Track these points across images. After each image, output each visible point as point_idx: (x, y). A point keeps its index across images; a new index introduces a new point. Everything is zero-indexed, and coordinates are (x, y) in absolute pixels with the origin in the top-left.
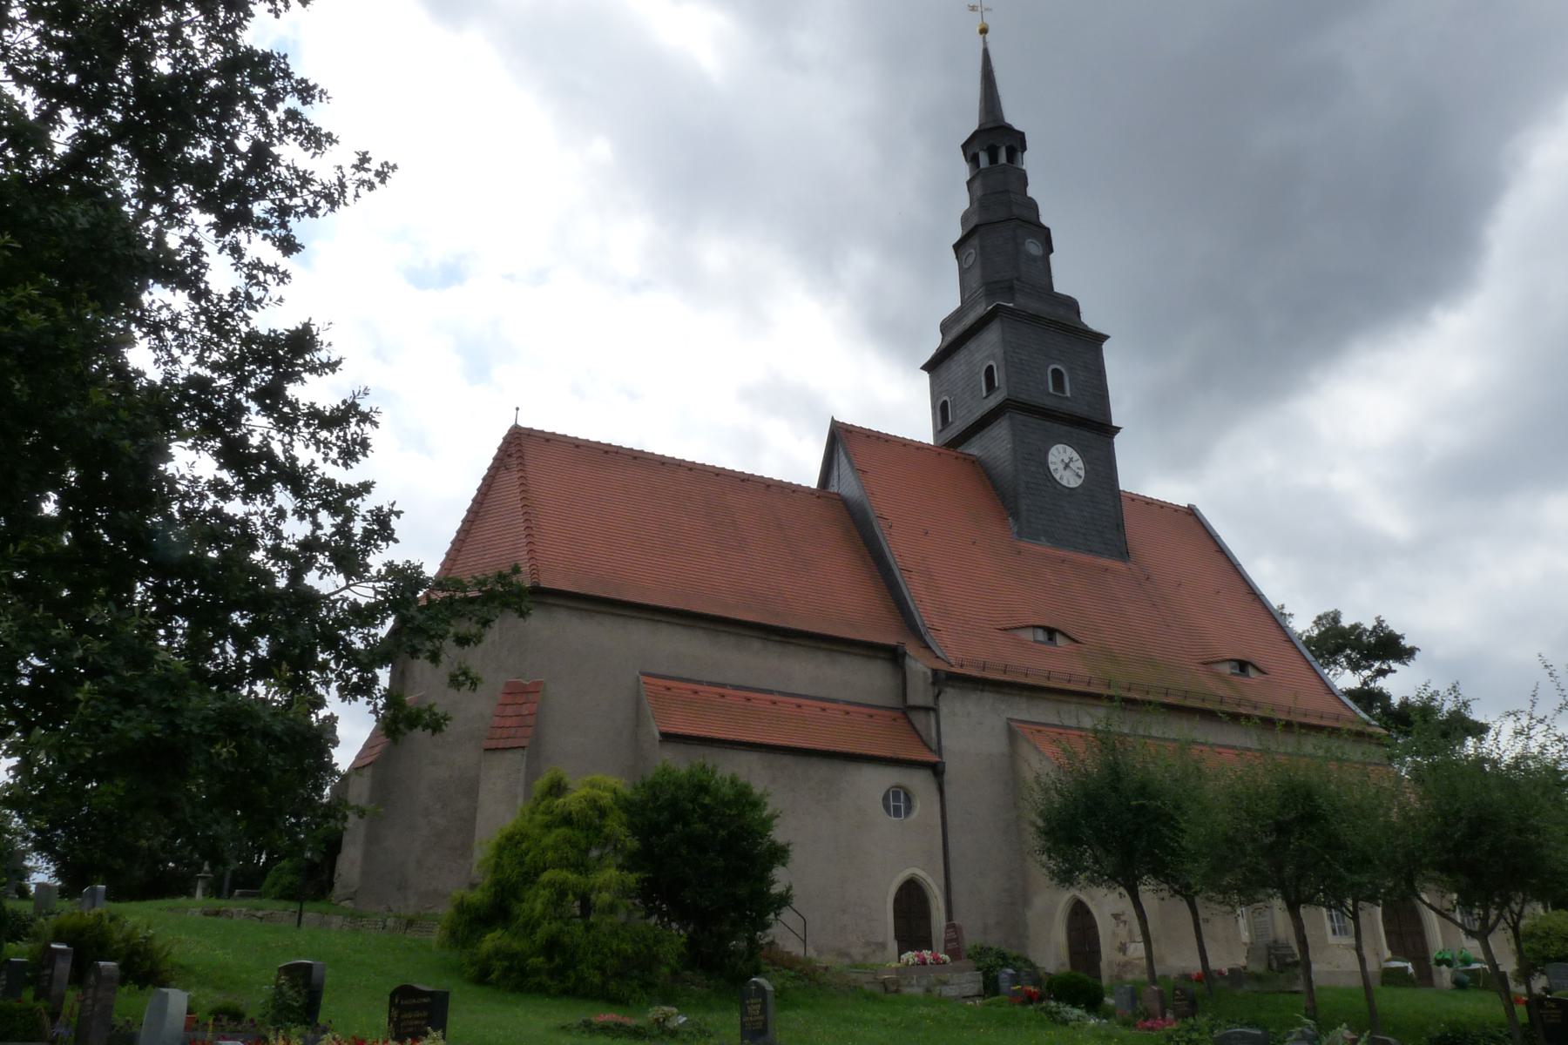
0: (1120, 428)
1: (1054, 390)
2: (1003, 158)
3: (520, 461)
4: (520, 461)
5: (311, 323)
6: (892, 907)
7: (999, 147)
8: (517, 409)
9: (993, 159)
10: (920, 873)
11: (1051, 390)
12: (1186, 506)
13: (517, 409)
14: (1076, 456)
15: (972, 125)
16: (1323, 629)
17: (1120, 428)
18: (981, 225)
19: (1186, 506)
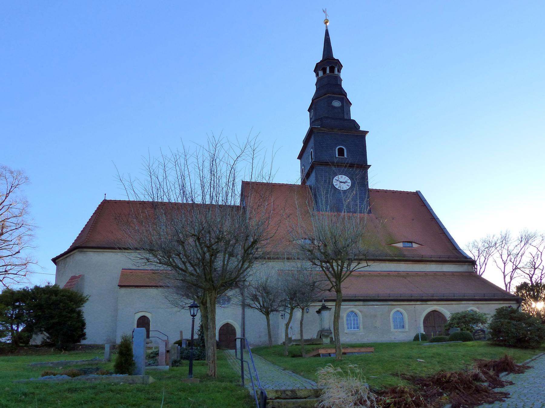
0: (371, 165)
1: (339, 155)
2: (328, 71)
3: (149, 345)
4: (149, 345)
5: (340, 245)
6: (218, 331)
7: (326, 67)
8: (105, 194)
9: (325, 72)
10: (230, 321)
11: (337, 156)
12: (415, 192)
13: (105, 194)
14: (334, 180)
15: (320, 58)
16: (185, 202)
17: (371, 165)
18: (314, 100)
19: (415, 192)
